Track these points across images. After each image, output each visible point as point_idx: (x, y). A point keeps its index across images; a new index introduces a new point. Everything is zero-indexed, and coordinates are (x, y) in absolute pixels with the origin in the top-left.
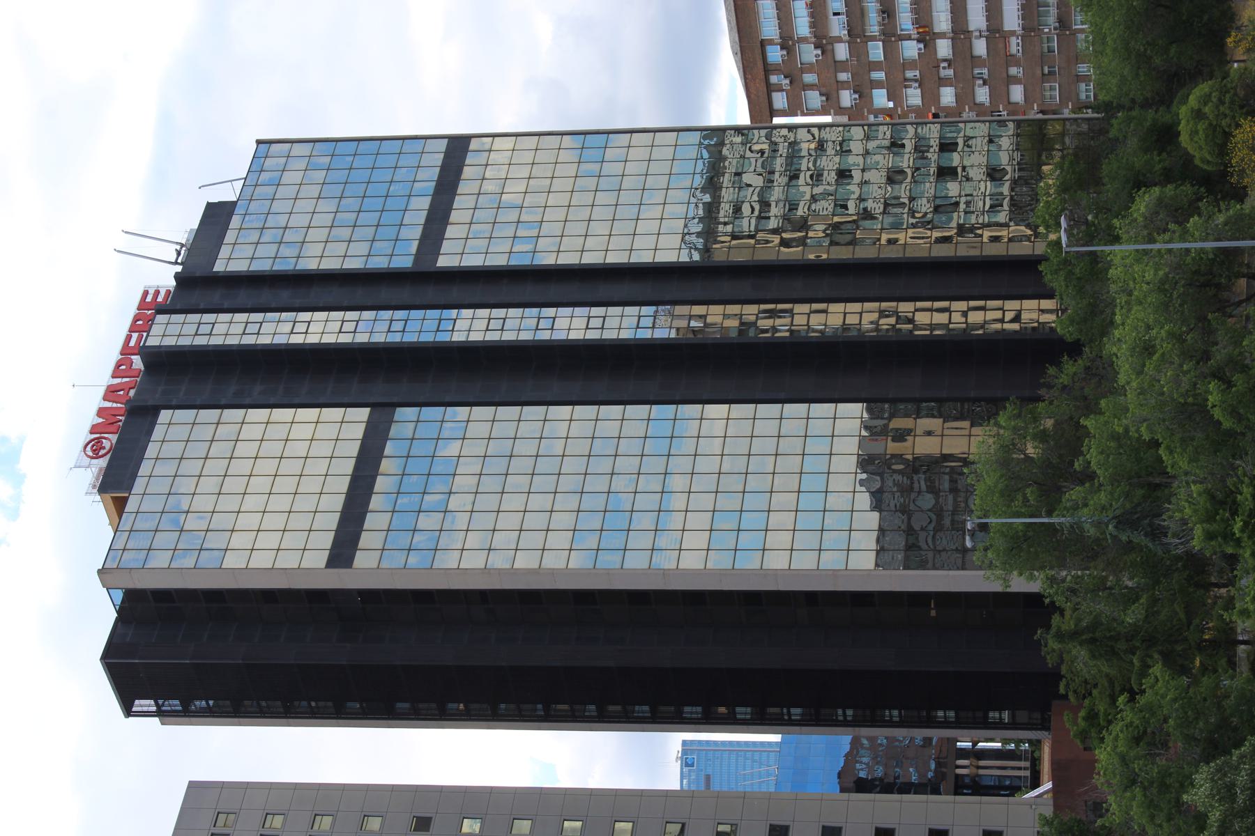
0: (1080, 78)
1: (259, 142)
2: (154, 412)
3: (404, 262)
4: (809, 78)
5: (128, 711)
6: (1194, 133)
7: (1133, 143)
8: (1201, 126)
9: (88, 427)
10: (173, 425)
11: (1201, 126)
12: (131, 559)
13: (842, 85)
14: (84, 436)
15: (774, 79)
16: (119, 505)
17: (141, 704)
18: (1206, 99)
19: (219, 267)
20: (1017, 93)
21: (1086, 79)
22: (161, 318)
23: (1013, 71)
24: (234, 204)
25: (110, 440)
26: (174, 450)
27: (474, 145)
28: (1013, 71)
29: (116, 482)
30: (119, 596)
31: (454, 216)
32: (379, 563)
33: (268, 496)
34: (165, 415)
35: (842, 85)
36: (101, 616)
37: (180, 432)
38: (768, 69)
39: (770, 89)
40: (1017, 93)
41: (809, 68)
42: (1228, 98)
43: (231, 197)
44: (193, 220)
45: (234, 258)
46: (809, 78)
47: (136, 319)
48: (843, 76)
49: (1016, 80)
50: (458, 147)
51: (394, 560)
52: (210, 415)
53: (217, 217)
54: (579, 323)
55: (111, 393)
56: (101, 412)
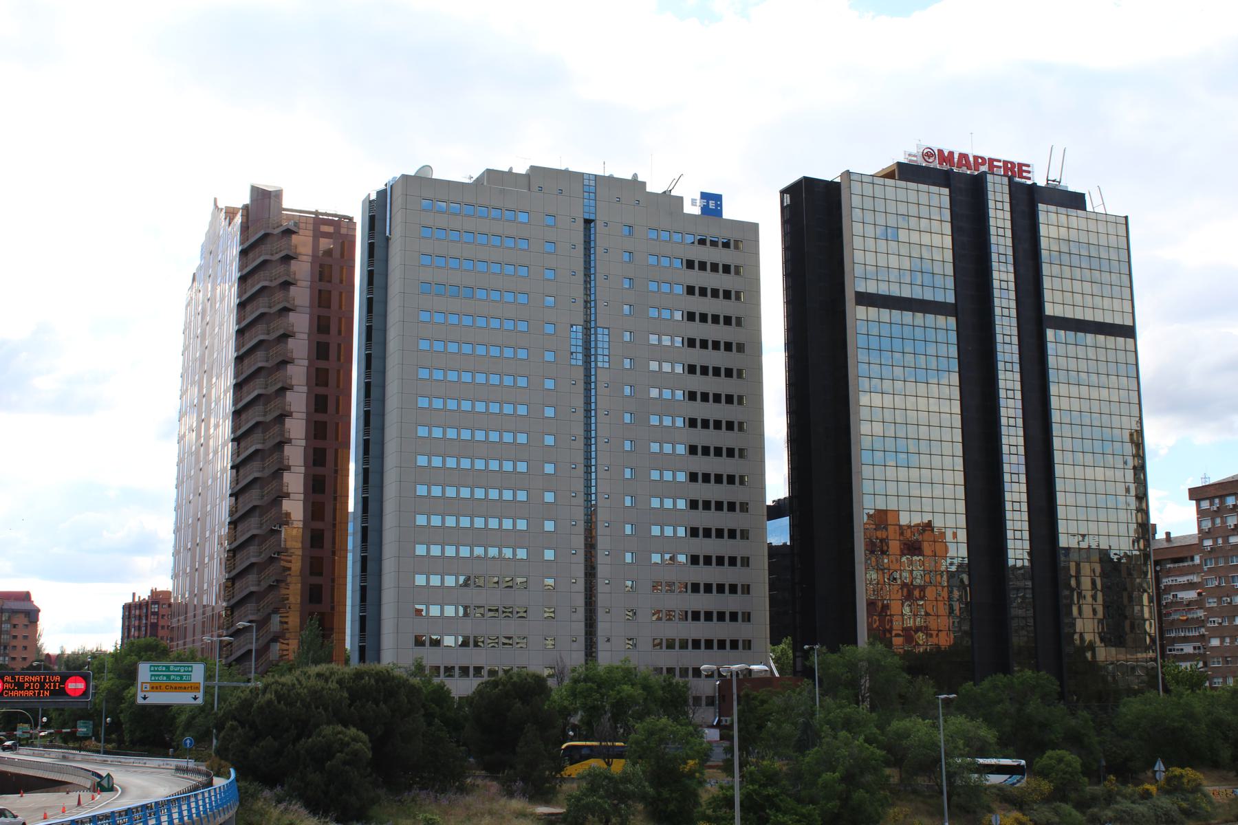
0: (1225, 678)
1: (1126, 218)
2: (946, 184)
3: (1049, 310)
4: (1218, 521)
5: (783, 192)
6: (1051, 758)
7: (1073, 722)
8: (1053, 762)
9: (941, 147)
10: (941, 196)
11: (1053, 762)
12: (856, 188)
13: (1215, 541)
14: (936, 146)
15: (1217, 501)
16: (889, 175)
17: (787, 198)
18: (1069, 765)
19: (1041, 207)
20: (1215, 642)
21: (1225, 681)
22: (1006, 180)
23: (1228, 640)
24: (1084, 208)
25: (935, 164)
26: (924, 199)
27: (1130, 341)
28: (1228, 640)
29: (905, 172)
30: (838, 180)
31: (1080, 335)
32: (859, 315)
33: (900, 250)
34: (946, 191)
35: (1215, 541)
36: (829, 173)
37: (935, 201)
38: (1222, 498)
39: (1211, 499)
40: (1215, 642)
41: (1224, 522)
42: (1068, 776)
43: (1089, 208)
44: (1073, 187)
45: (1051, 222)
46: (1218, 521)
47: (1012, 163)
48: (1220, 541)
49: (1222, 641)
50: (1128, 332)
51: (862, 328)
52: (947, 215)
53: (1076, 201)
54: (1012, 413)
55: (963, 156)
56: (951, 153)
